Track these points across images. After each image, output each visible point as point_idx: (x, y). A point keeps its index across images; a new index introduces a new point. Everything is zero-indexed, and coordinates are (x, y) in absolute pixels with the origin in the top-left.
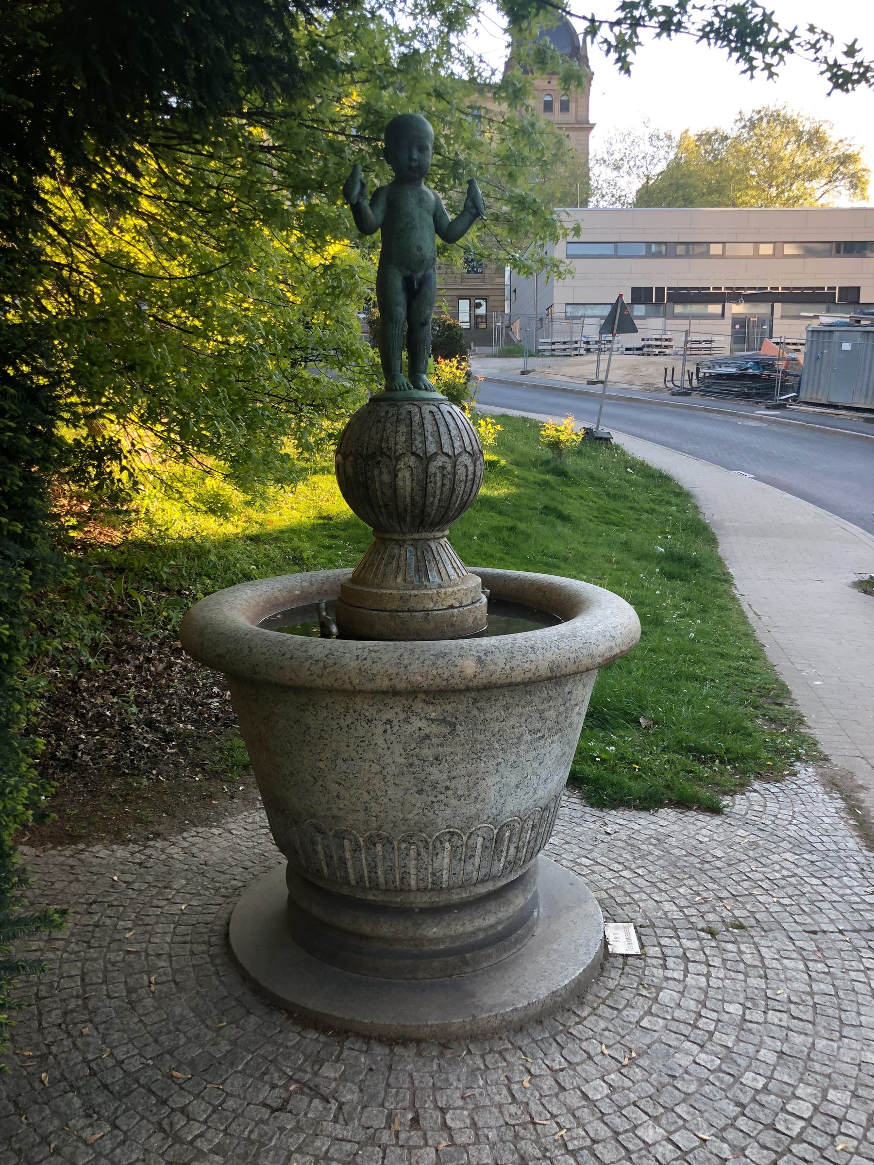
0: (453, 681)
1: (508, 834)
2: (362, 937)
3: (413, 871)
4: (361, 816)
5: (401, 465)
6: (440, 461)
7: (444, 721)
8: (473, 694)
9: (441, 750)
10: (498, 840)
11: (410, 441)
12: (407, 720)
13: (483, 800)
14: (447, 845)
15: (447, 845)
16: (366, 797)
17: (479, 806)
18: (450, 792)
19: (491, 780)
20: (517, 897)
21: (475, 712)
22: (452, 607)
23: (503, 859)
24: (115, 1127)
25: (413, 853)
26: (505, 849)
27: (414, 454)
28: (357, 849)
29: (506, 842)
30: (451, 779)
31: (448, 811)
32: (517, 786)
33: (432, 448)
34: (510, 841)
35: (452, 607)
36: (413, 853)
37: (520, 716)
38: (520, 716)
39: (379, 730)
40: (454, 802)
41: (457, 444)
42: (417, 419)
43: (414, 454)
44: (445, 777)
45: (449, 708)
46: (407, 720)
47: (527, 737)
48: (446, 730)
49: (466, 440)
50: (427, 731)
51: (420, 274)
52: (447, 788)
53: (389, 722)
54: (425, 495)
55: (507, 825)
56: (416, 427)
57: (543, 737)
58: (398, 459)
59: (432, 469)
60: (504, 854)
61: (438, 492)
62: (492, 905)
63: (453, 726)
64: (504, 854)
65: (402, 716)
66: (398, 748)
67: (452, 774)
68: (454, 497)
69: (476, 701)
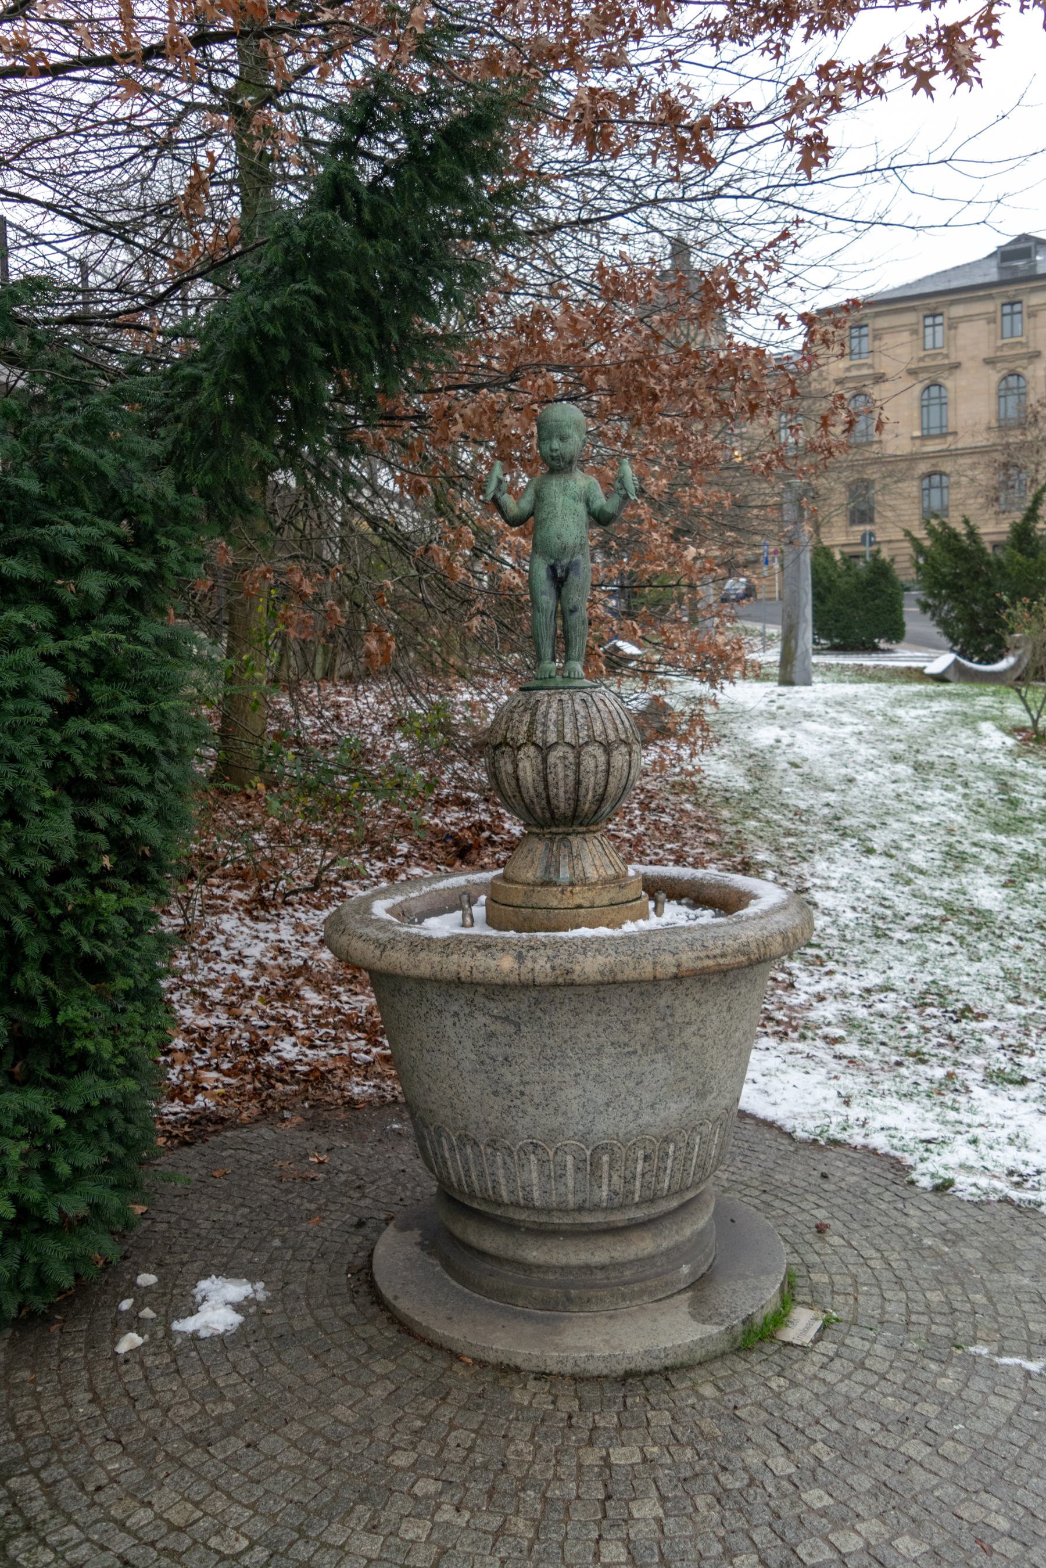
0: (489, 975)
1: (605, 1158)
2: (528, 1267)
3: (503, 1181)
4: (448, 1111)
5: (521, 755)
6: (559, 752)
7: (506, 1019)
8: (534, 994)
9: (509, 1051)
10: (595, 1165)
11: (530, 733)
12: (471, 1014)
13: (565, 1113)
14: (532, 1157)
15: (532, 1157)
16: (450, 1093)
17: (561, 1119)
18: (526, 1098)
19: (573, 1092)
20: (643, 1239)
21: (539, 1014)
22: (580, 907)
23: (605, 1187)
24: (174, 1361)
25: (499, 1160)
26: (605, 1175)
27: (534, 744)
28: (452, 1149)
29: (606, 1167)
30: (525, 1083)
31: (528, 1119)
32: (608, 1105)
33: (612, 737)
34: (611, 1167)
35: (580, 907)
36: (499, 1160)
37: (597, 1024)
38: (597, 1024)
39: (449, 1022)
40: (531, 1110)
41: (583, 733)
42: (543, 708)
43: (534, 744)
44: (517, 1080)
45: (510, 1005)
46: (471, 1014)
47: (609, 1050)
48: (511, 1029)
49: (609, 725)
50: (492, 1028)
51: (565, 561)
52: (522, 1094)
53: (456, 1014)
54: (546, 787)
55: (603, 1148)
56: (539, 717)
57: (635, 1052)
58: (519, 748)
59: (551, 759)
60: (605, 1181)
61: (561, 783)
62: (606, 1241)
63: (518, 1026)
64: (605, 1181)
65: (467, 1010)
66: (468, 1043)
67: (526, 1078)
68: (582, 791)
69: (537, 1002)
